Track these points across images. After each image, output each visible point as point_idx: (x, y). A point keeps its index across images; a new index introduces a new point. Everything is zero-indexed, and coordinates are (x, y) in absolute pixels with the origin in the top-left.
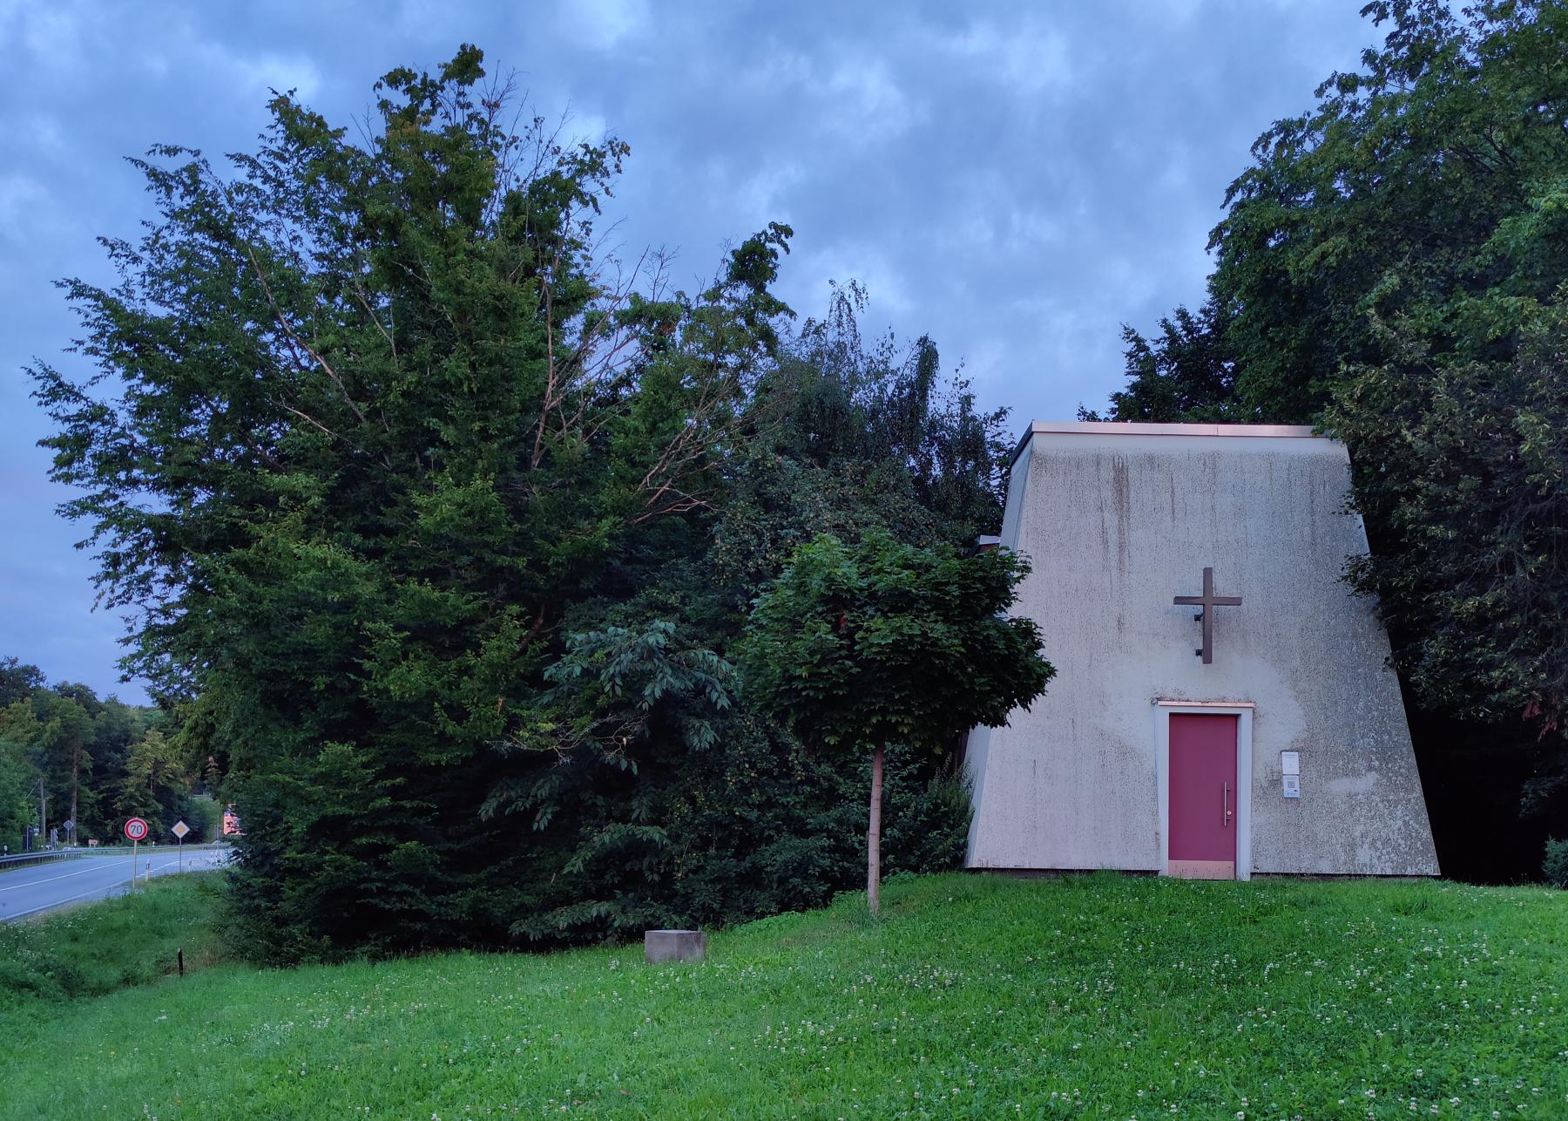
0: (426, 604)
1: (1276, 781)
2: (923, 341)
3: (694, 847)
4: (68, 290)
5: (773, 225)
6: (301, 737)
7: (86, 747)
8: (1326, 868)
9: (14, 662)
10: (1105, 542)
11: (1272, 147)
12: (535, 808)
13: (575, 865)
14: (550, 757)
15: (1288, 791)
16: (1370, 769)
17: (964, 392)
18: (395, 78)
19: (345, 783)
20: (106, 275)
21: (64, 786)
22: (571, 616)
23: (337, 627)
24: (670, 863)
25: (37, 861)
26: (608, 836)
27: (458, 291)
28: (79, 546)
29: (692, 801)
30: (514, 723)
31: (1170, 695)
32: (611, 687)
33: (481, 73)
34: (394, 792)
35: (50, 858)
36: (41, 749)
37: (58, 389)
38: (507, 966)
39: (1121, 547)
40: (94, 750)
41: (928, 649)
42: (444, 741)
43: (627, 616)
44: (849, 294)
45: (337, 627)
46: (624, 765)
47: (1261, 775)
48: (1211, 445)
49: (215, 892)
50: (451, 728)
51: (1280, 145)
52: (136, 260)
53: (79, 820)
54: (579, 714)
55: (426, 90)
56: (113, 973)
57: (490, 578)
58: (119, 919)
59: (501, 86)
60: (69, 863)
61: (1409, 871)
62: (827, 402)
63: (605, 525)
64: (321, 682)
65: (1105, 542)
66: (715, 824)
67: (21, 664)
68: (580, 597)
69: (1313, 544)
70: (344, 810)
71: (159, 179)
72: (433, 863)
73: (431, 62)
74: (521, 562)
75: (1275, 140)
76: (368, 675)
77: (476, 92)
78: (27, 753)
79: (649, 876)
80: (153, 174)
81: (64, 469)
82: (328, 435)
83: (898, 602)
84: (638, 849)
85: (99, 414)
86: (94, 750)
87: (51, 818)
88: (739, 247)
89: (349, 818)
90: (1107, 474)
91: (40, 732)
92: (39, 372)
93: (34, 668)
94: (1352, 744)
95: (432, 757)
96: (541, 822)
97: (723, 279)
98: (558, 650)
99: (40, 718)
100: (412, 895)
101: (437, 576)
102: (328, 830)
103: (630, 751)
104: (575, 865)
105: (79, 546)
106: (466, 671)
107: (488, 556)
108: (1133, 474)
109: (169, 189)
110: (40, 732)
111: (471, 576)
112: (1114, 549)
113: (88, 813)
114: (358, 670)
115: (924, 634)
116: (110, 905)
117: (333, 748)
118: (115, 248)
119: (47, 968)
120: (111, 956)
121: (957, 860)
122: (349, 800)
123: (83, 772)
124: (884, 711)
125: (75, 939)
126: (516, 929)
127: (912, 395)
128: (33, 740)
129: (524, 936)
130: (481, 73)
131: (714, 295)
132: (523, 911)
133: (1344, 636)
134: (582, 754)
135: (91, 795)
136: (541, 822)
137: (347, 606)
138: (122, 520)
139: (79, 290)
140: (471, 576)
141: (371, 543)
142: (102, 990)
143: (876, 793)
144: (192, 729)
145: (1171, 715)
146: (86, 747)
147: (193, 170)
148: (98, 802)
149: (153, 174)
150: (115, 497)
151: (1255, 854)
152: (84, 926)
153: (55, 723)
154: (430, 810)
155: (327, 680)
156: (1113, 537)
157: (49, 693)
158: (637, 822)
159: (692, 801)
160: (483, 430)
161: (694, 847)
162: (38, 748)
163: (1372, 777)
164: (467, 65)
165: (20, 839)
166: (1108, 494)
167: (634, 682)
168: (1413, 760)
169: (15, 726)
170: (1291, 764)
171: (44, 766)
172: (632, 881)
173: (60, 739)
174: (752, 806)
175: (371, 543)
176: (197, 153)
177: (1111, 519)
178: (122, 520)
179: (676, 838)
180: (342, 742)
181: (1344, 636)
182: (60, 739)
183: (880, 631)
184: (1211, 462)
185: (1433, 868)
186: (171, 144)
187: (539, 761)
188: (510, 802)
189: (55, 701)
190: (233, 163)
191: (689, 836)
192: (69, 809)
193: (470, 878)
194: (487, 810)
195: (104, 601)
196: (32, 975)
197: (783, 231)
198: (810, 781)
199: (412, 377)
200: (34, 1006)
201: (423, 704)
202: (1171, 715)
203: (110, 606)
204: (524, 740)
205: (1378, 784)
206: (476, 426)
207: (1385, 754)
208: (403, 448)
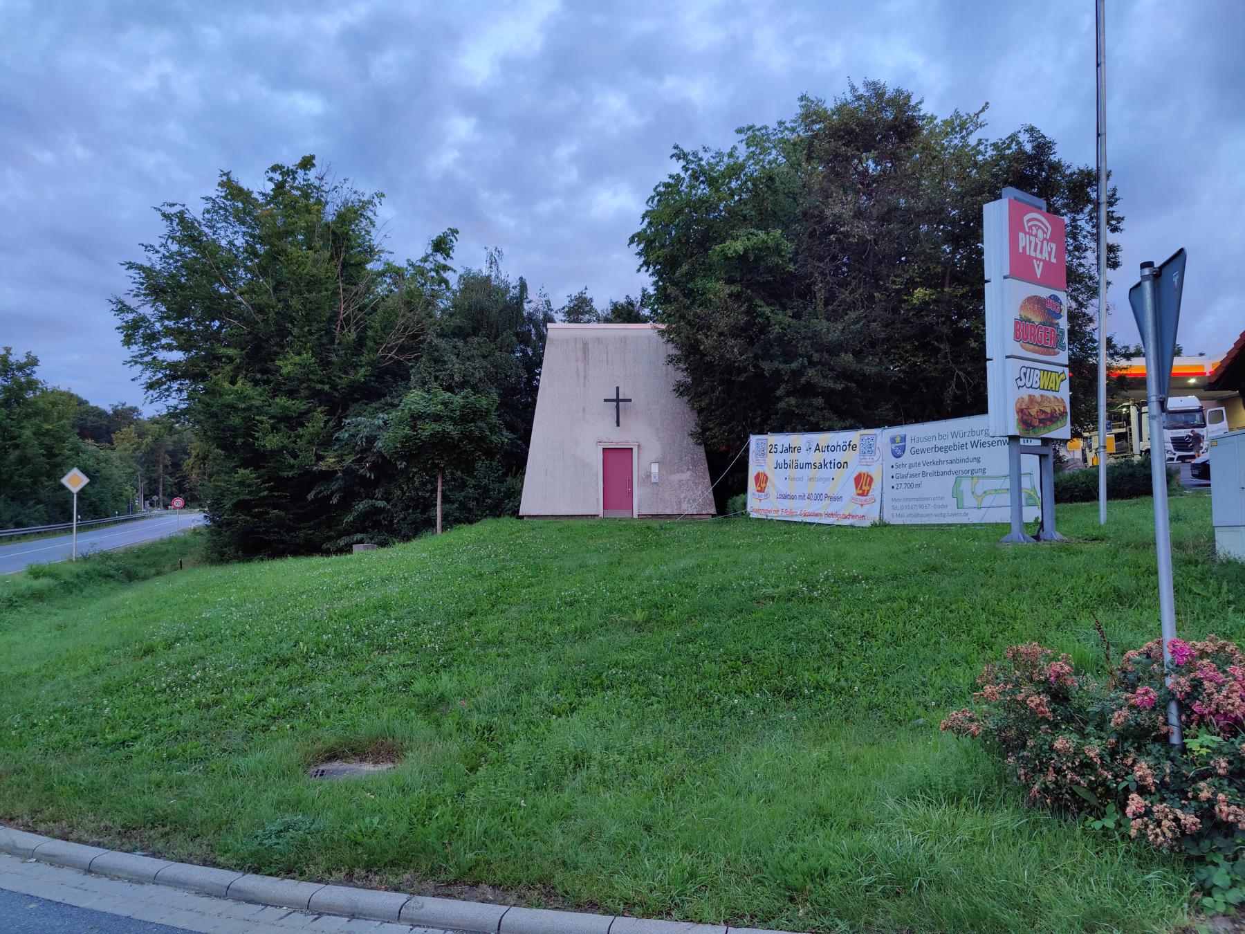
0: (283, 407)
1: (649, 476)
2: (521, 278)
3: (403, 509)
4: (126, 266)
5: (449, 229)
6: (233, 464)
7: (167, 452)
8: (668, 512)
9: (124, 405)
10: (578, 375)
11: (655, 202)
12: (332, 494)
13: (350, 518)
14: (336, 472)
15: (653, 480)
16: (688, 469)
17: (546, 298)
18: (274, 169)
19: (249, 486)
20: (144, 259)
21: (154, 475)
22: (351, 409)
23: (244, 418)
24: (392, 516)
25: (135, 519)
26: (362, 506)
27: (294, 274)
28: (133, 380)
29: (402, 489)
30: (320, 458)
31: (605, 440)
32: (360, 442)
33: (313, 165)
34: (269, 489)
35: (148, 517)
36: (140, 455)
37: (123, 308)
38: (317, 560)
39: (585, 378)
40: (172, 454)
41: (445, 435)
42: (292, 467)
43: (376, 409)
44: (496, 255)
45: (244, 418)
46: (368, 475)
47: (642, 473)
48: (624, 333)
49: (200, 534)
50: (292, 461)
51: (659, 201)
52: (158, 252)
53: (164, 495)
54: (350, 453)
55: (288, 173)
56: (153, 571)
57: (315, 394)
58: (164, 548)
59: (324, 169)
60: (157, 519)
61: (704, 512)
62: (478, 306)
63: (362, 371)
64: (240, 441)
65: (578, 375)
66: (411, 499)
67: (128, 405)
68: (356, 401)
69: (667, 374)
70: (248, 497)
71: (167, 217)
72: (289, 519)
73: (291, 161)
74: (326, 387)
75: (656, 199)
76: (257, 439)
77: (312, 175)
78: (132, 457)
79: (383, 522)
80: (164, 215)
81: (128, 341)
82: (246, 329)
83: (437, 418)
84: (380, 511)
85: (143, 319)
86: (172, 454)
87: (147, 493)
88: (434, 238)
89: (250, 501)
90: (580, 346)
91: (140, 444)
92: (114, 300)
93: (136, 408)
94: (681, 459)
95: (285, 474)
96: (334, 501)
97: (430, 251)
98: (339, 426)
99: (139, 437)
100: (279, 533)
101: (292, 394)
102: (241, 506)
103: (370, 470)
104: (350, 518)
105: (133, 380)
106: (300, 437)
107: (313, 385)
108: (590, 346)
109: (172, 220)
110: (140, 444)
111: (307, 393)
112: (582, 379)
113: (169, 490)
114: (253, 436)
115: (444, 430)
116: (162, 542)
117: (241, 471)
118: (147, 247)
119: (120, 569)
120: (154, 565)
121: (515, 513)
122: (250, 493)
123: (166, 467)
124: (433, 459)
125: (138, 557)
126: (324, 546)
127: (517, 303)
128: (135, 450)
129: (329, 549)
130: (313, 165)
131: (425, 260)
132: (329, 539)
133: (679, 413)
134: (348, 472)
135: (170, 480)
136: (334, 501)
137: (249, 409)
138: (155, 364)
139: (131, 266)
140: (307, 393)
141: (265, 377)
142: (145, 578)
143: (439, 489)
144: (196, 457)
145: (604, 449)
146: (167, 452)
147: (182, 213)
148: (175, 484)
149: (164, 215)
150: (152, 354)
151: (639, 506)
152: (143, 552)
153: (149, 439)
154: (286, 496)
155: (242, 440)
156: (582, 373)
157: (145, 422)
158: (377, 499)
159: (402, 489)
160: (309, 330)
161: (403, 509)
162: (138, 454)
163: (689, 473)
164: (307, 163)
165: (126, 507)
166: (580, 355)
167: (371, 440)
168: (706, 466)
169: (125, 442)
170: (655, 468)
171: (142, 465)
172: (377, 525)
173: (152, 448)
174: (427, 491)
175: (265, 377)
176: (184, 206)
177: (581, 365)
178: (155, 364)
179: (395, 506)
180: (245, 469)
181: (679, 413)
182: (152, 448)
183: (428, 429)
184: (624, 340)
185: (713, 511)
186: (171, 202)
187: (329, 475)
188: (321, 492)
189: (147, 426)
190: (204, 201)
191: (400, 505)
192: (158, 488)
193: (303, 525)
194: (311, 496)
195: (149, 400)
196: (112, 572)
197: (454, 232)
198: (453, 479)
199: (280, 306)
200: (113, 584)
201: (277, 453)
202: (604, 449)
203: (152, 402)
204: (322, 466)
205: (691, 476)
206: (306, 329)
207: (695, 464)
208: (278, 336)
